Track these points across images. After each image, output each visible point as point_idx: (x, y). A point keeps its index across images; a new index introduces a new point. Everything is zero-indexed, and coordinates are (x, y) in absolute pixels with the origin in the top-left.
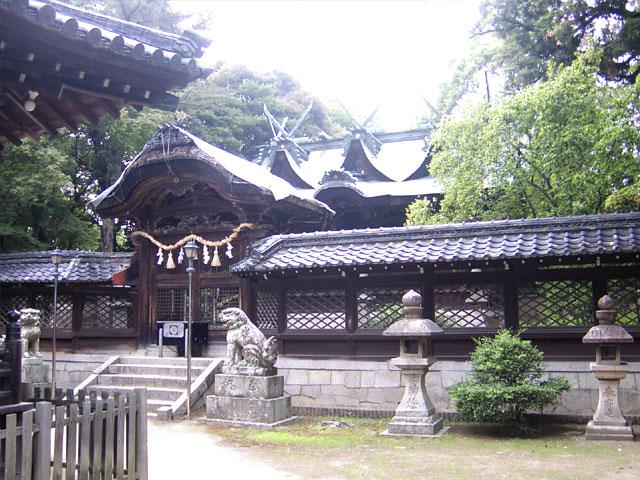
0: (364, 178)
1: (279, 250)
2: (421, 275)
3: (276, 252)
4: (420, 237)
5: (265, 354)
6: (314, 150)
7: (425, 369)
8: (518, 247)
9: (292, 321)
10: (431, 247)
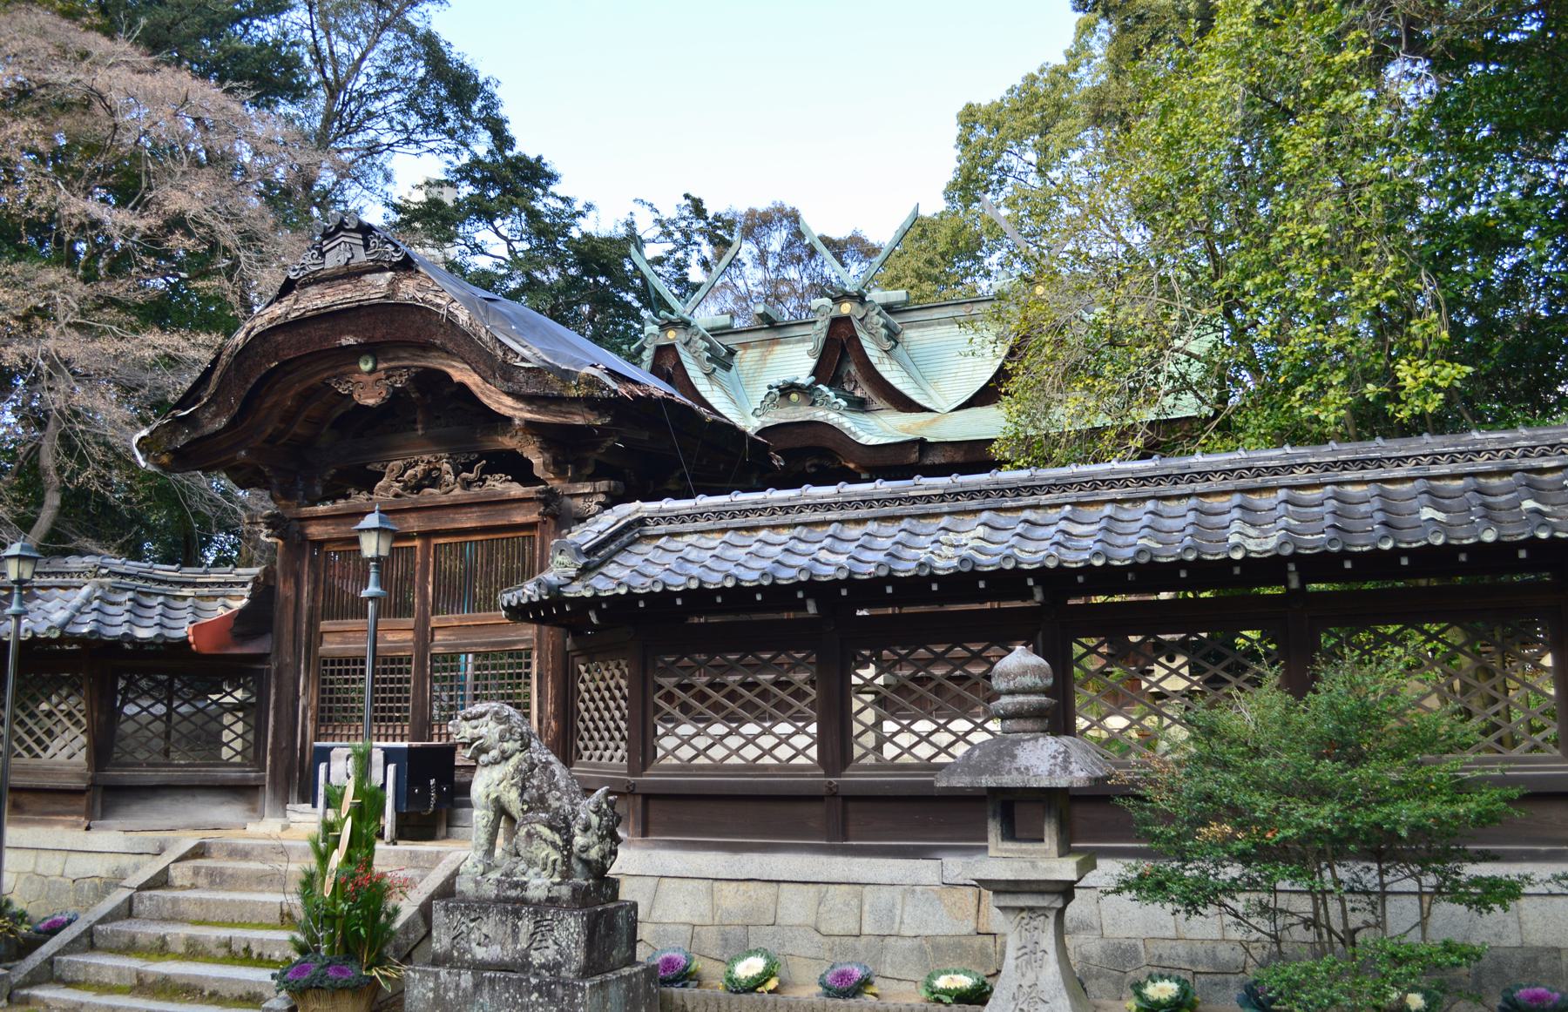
0: (860, 405)
1: (633, 542)
2: (810, 621)
3: (623, 549)
4: (1031, 500)
5: (579, 840)
6: (745, 346)
7: (1066, 891)
8: (1329, 520)
9: (669, 742)
10: (1063, 525)
